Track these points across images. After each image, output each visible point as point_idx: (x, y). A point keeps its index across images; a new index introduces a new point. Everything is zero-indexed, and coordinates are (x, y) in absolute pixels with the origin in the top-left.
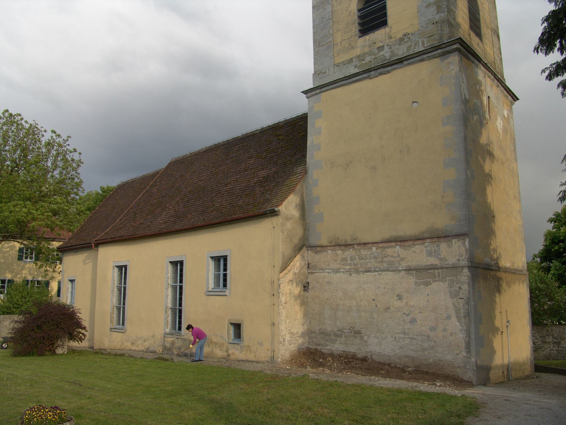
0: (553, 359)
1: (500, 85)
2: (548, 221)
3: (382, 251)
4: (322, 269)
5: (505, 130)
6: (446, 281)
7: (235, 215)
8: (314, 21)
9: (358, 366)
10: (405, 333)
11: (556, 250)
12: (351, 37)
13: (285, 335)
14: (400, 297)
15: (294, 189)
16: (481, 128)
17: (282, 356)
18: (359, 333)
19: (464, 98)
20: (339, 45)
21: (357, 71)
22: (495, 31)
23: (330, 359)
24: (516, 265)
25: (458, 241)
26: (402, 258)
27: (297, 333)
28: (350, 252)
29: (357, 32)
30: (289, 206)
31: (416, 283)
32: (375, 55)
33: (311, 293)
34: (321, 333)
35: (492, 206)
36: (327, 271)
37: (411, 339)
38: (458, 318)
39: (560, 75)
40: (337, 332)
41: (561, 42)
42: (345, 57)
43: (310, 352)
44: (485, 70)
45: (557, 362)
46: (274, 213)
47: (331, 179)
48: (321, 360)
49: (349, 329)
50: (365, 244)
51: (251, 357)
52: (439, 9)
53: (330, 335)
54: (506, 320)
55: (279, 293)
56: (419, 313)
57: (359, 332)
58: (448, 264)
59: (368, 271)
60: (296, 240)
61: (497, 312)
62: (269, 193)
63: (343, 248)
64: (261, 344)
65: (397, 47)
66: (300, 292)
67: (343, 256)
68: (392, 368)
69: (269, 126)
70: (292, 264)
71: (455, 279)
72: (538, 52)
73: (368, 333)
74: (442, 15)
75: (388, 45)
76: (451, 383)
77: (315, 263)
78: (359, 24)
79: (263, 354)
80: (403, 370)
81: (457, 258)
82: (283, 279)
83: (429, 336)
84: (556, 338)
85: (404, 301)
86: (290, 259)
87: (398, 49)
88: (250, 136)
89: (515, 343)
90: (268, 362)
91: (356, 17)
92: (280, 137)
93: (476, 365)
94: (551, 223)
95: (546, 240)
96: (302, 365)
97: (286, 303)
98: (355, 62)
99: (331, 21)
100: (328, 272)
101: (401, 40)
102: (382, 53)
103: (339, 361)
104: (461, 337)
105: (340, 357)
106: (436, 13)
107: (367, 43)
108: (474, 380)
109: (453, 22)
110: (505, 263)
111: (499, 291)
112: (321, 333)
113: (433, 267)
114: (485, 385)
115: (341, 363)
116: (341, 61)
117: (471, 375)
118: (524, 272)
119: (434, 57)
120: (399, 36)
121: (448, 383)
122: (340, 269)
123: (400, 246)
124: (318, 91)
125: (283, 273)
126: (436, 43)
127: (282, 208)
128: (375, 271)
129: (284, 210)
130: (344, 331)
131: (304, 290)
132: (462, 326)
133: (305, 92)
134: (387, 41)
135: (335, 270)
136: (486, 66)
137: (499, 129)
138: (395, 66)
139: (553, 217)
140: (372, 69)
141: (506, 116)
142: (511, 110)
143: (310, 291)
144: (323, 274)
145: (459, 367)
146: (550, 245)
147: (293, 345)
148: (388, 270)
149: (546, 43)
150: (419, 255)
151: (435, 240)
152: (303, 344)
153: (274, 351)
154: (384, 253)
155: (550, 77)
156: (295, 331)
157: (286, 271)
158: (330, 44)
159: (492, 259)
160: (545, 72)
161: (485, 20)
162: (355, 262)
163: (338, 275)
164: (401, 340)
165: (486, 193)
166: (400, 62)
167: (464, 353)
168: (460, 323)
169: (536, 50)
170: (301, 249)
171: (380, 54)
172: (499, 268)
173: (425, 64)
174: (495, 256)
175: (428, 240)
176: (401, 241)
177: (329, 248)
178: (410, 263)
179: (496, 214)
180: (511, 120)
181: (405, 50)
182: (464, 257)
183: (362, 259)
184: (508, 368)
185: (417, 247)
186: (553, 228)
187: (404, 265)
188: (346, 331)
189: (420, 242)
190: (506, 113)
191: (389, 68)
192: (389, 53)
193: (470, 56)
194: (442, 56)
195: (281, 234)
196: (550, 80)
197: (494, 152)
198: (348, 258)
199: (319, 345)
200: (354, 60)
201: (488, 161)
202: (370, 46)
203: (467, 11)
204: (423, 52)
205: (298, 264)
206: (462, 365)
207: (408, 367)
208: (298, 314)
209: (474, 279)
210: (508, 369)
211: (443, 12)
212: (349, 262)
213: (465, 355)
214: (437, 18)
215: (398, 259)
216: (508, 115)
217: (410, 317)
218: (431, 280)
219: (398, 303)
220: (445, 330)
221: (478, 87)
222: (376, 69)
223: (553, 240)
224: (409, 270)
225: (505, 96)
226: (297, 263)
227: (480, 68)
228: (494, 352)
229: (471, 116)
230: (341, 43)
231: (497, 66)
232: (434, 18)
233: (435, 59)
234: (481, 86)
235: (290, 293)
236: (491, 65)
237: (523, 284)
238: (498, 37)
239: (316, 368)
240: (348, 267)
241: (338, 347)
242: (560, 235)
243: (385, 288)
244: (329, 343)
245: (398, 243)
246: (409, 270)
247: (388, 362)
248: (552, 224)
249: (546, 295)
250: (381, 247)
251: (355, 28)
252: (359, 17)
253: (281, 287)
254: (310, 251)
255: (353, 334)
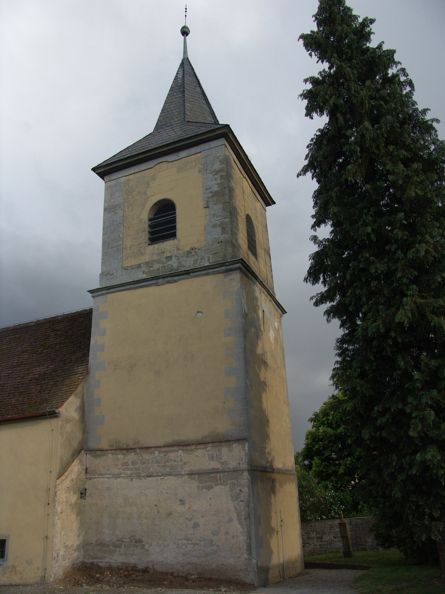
0: (317, 554)
1: (272, 300)
2: (308, 421)
3: (165, 455)
4: (101, 474)
5: (276, 340)
6: (227, 484)
7: (8, 415)
8: (104, 223)
9: (139, 578)
10: (188, 539)
11: (317, 449)
12: (141, 243)
13: (59, 550)
14: (182, 502)
15: (75, 390)
16: (258, 339)
17: (55, 575)
18: (140, 542)
19: (244, 311)
20: (128, 250)
21: (144, 276)
22: (267, 251)
23: (108, 573)
24: (286, 465)
25: (238, 445)
26: (184, 463)
27: (72, 545)
28: (132, 457)
29: (147, 240)
30: (70, 408)
31: (198, 487)
32: (163, 263)
33: (88, 500)
34: (98, 545)
35: (267, 412)
36: (107, 476)
37: (194, 544)
38: (240, 521)
39: (324, 303)
40: (117, 542)
41: (323, 276)
42: (134, 262)
43: (86, 567)
44: (260, 287)
45: (321, 556)
46: (53, 415)
47: (117, 381)
48: (98, 575)
49: (130, 538)
50: (147, 448)
51: (16, 579)
52: (224, 230)
53: (108, 546)
54: (280, 520)
55: (55, 501)
56: (202, 517)
57: (140, 541)
58: (229, 468)
59: (150, 476)
60: (75, 444)
61: (273, 514)
62: (46, 392)
63: (124, 452)
64: (29, 563)
65: (185, 259)
66: (77, 499)
67: (125, 461)
68: (175, 577)
69: (45, 319)
70: (69, 469)
71: (236, 482)
72: (307, 282)
73: (150, 541)
74: (226, 236)
75: (176, 256)
76: (235, 588)
77: (93, 468)
78: (150, 233)
79: (31, 575)
80: (186, 579)
81: (237, 461)
82: (60, 486)
83: (211, 541)
84: (319, 533)
85: (187, 506)
86: (68, 464)
87: (186, 261)
88: (24, 327)
89: (288, 543)
90: (37, 583)
91: (147, 226)
92: (59, 333)
93: (257, 566)
94: (311, 422)
95: (307, 439)
96: (77, 583)
97: (61, 513)
98: (144, 268)
99: (122, 225)
100: (108, 478)
101: (189, 253)
102: (170, 263)
103: (118, 574)
104: (242, 539)
105: (119, 569)
106: (221, 233)
107: (156, 252)
108: (255, 582)
109: (235, 243)
110: (278, 465)
111: (274, 492)
112: (98, 545)
113: (216, 471)
114: (265, 586)
115: (121, 577)
116: (129, 265)
117: (252, 577)
118: (294, 472)
119: (218, 273)
120: (187, 249)
121: (232, 587)
122: (121, 474)
123: (183, 450)
124: (104, 292)
125: (61, 479)
126: (220, 260)
127: (62, 410)
128: (157, 476)
129: (64, 411)
130: (124, 540)
131: (81, 497)
132: (243, 528)
133: (91, 292)
134: (176, 252)
135: (115, 475)
136: (261, 283)
137: (271, 339)
138: (182, 277)
139: (313, 417)
140: (160, 277)
141: (277, 327)
142: (280, 322)
143: (87, 498)
144: (102, 479)
145: (241, 570)
146: (311, 443)
147: (67, 560)
148: (170, 475)
149: (313, 275)
150: (201, 459)
151: (217, 444)
152: (78, 558)
153: (45, 569)
154: (167, 457)
155: (316, 304)
156: (70, 543)
157: (63, 477)
158: (119, 247)
159: (268, 462)
160: (312, 299)
161: (260, 242)
162: (137, 466)
163: (119, 480)
164: (184, 547)
165: (261, 399)
166: (187, 273)
167: (245, 556)
168: (242, 526)
169: (306, 280)
170: (79, 452)
171: (168, 264)
172: (273, 469)
173: (210, 279)
174: (270, 459)
175: (210, 445)
176: (183, 446)
177: (109, 452)
178: (192, 468)
179: (270, 419)
180: (280, 331)
181: (192, 263)
182: (244, 461)
183: (144, 463)
184: (283, 567)
185: (200, 451)
186: (313, 428)
187: (187, 469)
188: (126, 540)
189: (202, 446)
190: (276, 324)
191: (176, 278)
192: (177, 264)
193: (249, 274)
194: (225, 272)
195: (60, 437)
196: (317, 306)
197: (268, 361)
198: (130, 463)
199: (96, 558)
200: (142, 265)
201: (263, 370)
202: (158, 255)
203: (245, 233)
204: (208, 267)
205: (76, 469)
206: (244, 567)
207: (192, 575)
208: (74, 525)
209: (253, 481)
210: (283, 569)
211: (228, 233)
212: (130, 466)
213: (247, 557)
214: (222, 238)
215: (181, 463)
216: (278, 326)
217: (192, 522)
218: (214, 484)
219: (180, 508)
220: (227, 533)
221: (255, 302)
222: (163, 277)
223: (313, 438)
224: (191, 474)
225: (276, 309)
226: (76, 468)
227: (257, 286)
228: (271, 552)
229: (249, 328)
230: (130, 247)
231: (268, 282)
232: (220, 238)
233: (219, 275)
234: (257, 301)
235: (67, 502)
236: (265, 282)
237: (293, 483)
238: (270, 256)
239: (93, 585)
240: (129, 472)
241: (117, 559)
242: (320, 434)
243: (167, 493)
244: (106, 555)
245: (181, 448)
246: (191, 474)
247: (170, 571)
248: (312, 424)
249: (309, 492)
250: (163, 452)
251: (145, 236)
252: (150, 226)
253: (58, 495)
254: (88, 455)
255: (133, 543)
